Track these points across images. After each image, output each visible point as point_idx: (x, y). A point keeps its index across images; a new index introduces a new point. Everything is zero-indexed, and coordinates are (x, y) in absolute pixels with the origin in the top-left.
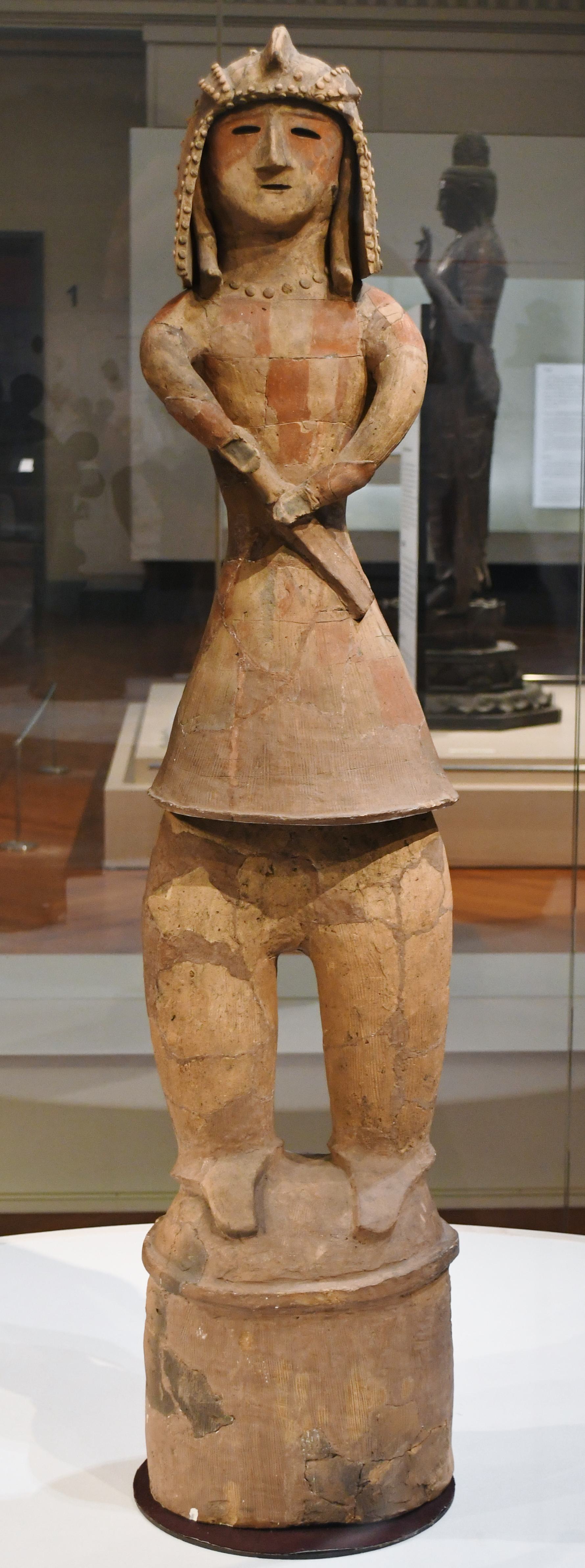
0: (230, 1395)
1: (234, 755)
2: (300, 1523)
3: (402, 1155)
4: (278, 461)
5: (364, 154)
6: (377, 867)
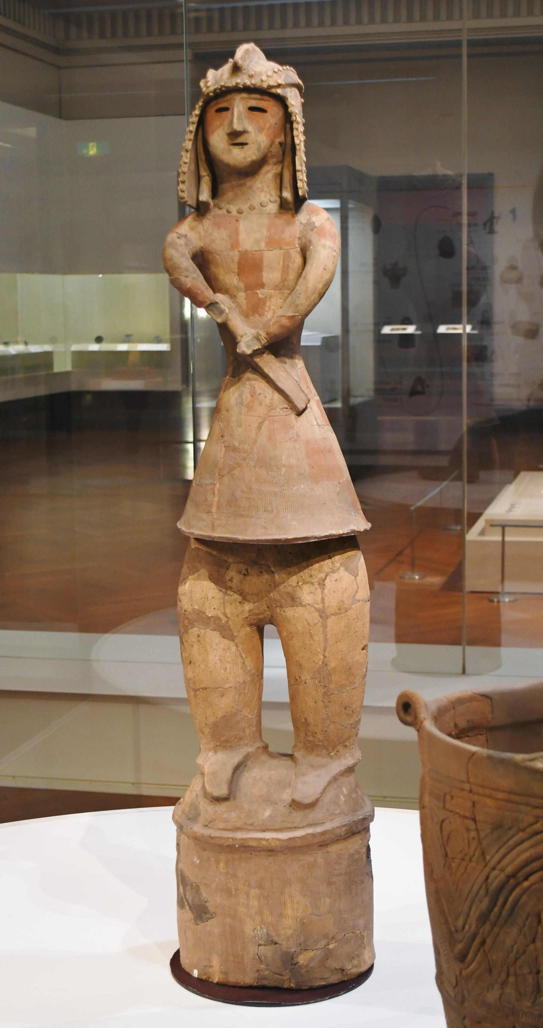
0: (214, 900)
1: (216, 499)
2: (255, 984)
3: (332, 756)
4: (246, 315)
5: (296, 121)
6: (309, 571)
